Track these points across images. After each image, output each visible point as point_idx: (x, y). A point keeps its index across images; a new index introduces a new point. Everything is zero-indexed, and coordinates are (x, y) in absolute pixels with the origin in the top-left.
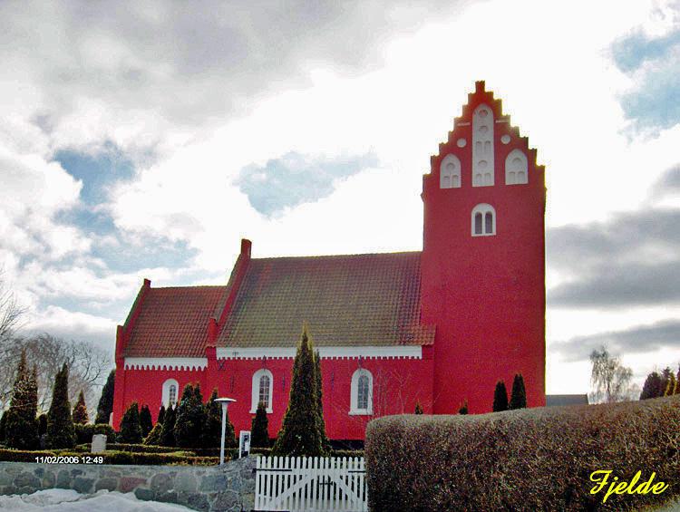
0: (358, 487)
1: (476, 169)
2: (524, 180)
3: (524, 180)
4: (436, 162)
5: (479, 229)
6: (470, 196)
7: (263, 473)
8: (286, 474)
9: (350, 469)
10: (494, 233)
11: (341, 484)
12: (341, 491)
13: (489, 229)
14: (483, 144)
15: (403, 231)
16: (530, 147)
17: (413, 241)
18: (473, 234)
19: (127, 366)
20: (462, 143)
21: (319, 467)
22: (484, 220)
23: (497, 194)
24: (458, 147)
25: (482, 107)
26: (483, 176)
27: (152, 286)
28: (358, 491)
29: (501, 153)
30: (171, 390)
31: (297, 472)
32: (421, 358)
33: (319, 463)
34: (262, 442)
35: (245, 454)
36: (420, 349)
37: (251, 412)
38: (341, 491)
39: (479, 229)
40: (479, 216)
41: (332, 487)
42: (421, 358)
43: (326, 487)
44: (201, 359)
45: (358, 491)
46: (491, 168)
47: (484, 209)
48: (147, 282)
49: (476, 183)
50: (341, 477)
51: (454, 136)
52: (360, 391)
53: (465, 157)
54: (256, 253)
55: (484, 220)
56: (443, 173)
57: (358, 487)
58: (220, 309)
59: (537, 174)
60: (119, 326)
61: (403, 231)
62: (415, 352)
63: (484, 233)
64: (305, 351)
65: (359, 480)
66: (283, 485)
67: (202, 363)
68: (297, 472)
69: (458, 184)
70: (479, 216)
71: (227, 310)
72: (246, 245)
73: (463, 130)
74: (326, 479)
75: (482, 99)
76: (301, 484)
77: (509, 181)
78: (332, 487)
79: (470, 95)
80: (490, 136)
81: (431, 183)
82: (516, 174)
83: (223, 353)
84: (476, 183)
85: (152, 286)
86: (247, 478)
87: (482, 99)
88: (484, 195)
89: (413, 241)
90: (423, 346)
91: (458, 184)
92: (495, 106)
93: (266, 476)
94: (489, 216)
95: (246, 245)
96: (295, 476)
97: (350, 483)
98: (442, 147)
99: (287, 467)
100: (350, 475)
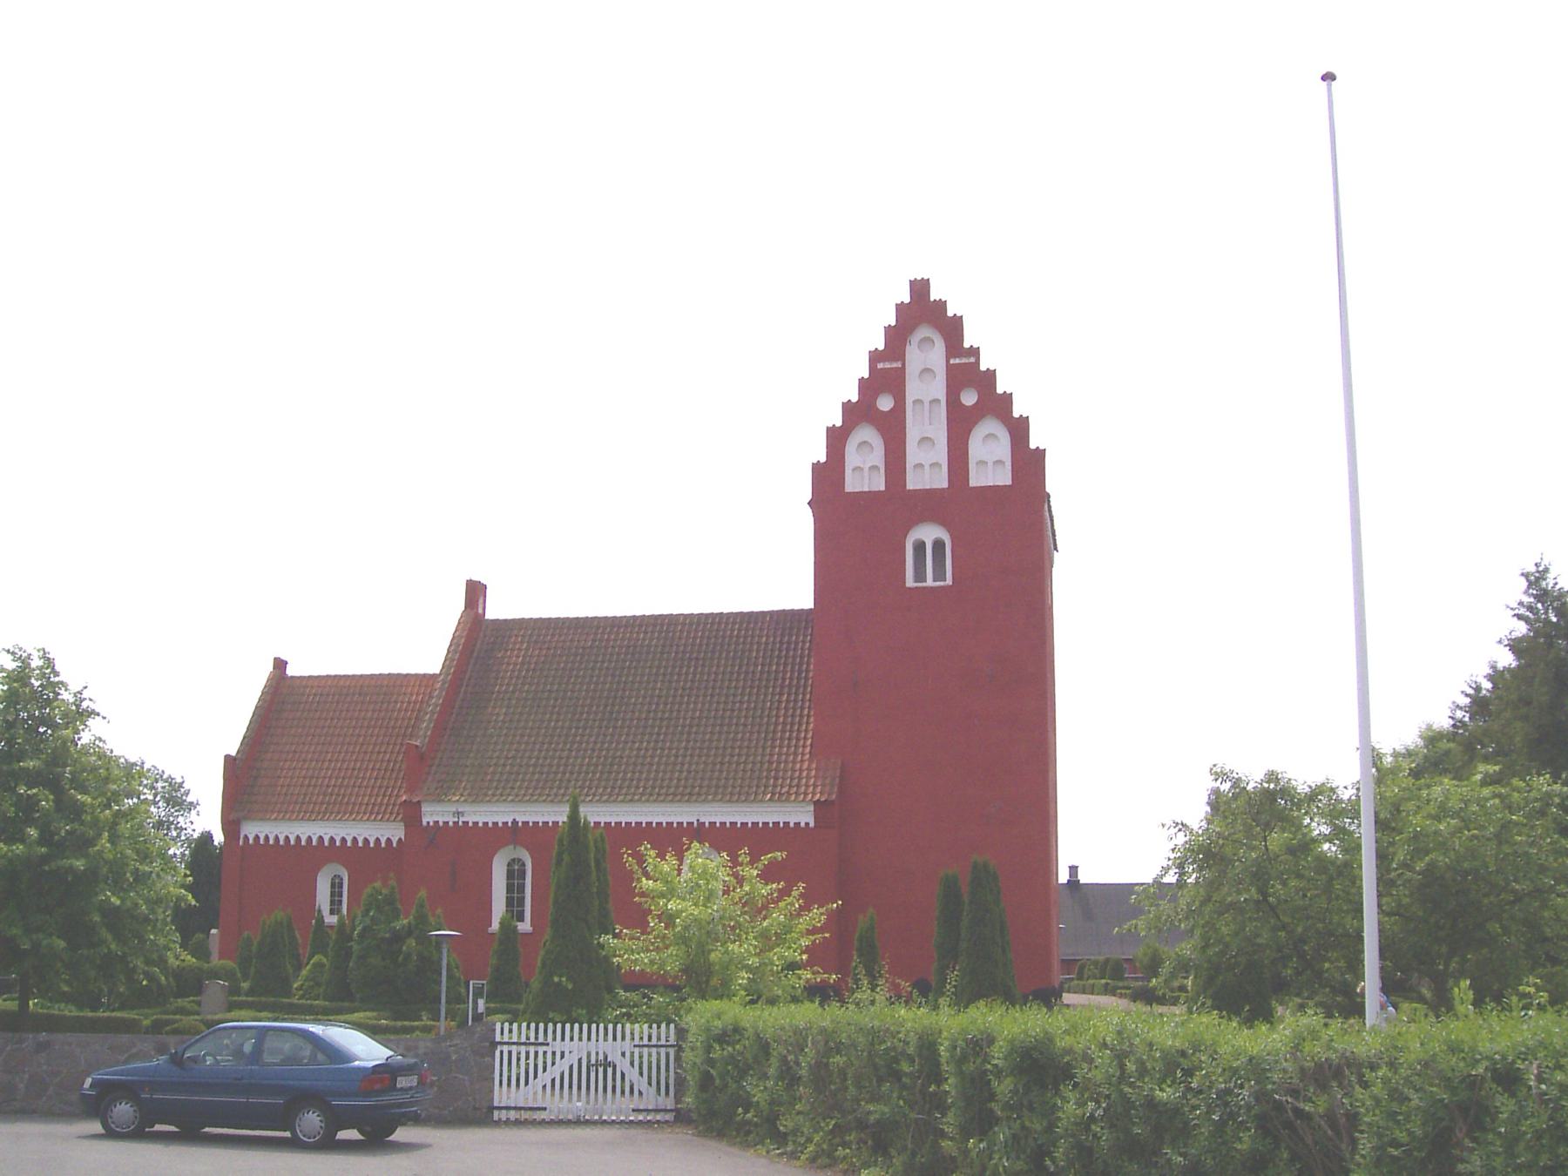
0: (614, 1079)
1: (914, 454)
2: (1004, 478)
3: (1004, 478)
4: (837, 439)
5: (920, 575)
6: (899, 504)
7: (506, 1049)
8: (541, 1050)
9: (637, 1042)
10: (949, 581)
11: (623, 1065)
12: (623, 1075)
13: (939, 573)
14: (927, 405)
15: (775, 571)
16: (1016, 414)
17: (793, 589)
18: (910, 582)
19: (246, 837)
20: (885, 403)
21: (615, 1039)
22: (927, 553)
23: (956, 502)
24: (877, 403)
25: (924, 331)
26: (927, 467)
27: (290, 672)
28: (650, 1077)
29: (960, 424)
30: (333, 885)
31: (558, 1046)
32: (812, 825)
33: (554, 1032)
34: (507, 995)
35: (478, 1018)
36: (812, 808)
37: (490, 930)
38: (623, 1075)
39: (920, 575)
40: (920, 547)
41: (610, 1070)
42: (812, 825)
43: (601, 1070)
44: (392, 825)
45: (650, 1077)
46: (940, 453)
47: (929, 533)
48: (280, 664)
49: (913, 482)
50: (623, 1054)
51: (869, 387)
52: (510, 888)
53: (893, 430)
54: (496, 609)
55: (927, 553)
56: (852, 457)
57: (614, 1079)
58: (426, 726)
59: (1029, 464)
60: (227, 758)
61: (775, 571)
62: (804, 816)
63: (930, 582)
64: (574, 816)
65: (641, 1057)
66: (536, 1066)
67: (393, 832)
68: (558, 1046)
69: (879, 484)
70: (920, 547)
71: (440, 727)
72: (475, 592)
73: (885, 374)
74: (601, 1057)
75: (922, 312)
76: (563, 1065)
77: (977, 479)
78: (610, 1070)
79: (900, 308)
80: (937, 388)
81: (827, 477)
82: (990, 461)
83: (434, 814)
84: (913, 482)
85: (290, 672)
86: (483, 1056)
87: (922, 312)
88: (929, 505)
89: (793, 589)
90: (816, 803)
91: (879, 484)
92: (952, 329)
93: (510, 1053)
94: (939, 545)
95: (475, 592)
96: (554, 1053)
97: (636, 1063)
98: (848, 407)
99: (541, 1040)
100: (637, 1050)
